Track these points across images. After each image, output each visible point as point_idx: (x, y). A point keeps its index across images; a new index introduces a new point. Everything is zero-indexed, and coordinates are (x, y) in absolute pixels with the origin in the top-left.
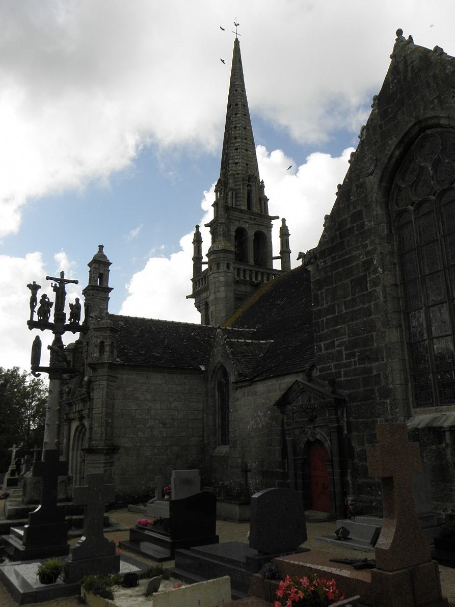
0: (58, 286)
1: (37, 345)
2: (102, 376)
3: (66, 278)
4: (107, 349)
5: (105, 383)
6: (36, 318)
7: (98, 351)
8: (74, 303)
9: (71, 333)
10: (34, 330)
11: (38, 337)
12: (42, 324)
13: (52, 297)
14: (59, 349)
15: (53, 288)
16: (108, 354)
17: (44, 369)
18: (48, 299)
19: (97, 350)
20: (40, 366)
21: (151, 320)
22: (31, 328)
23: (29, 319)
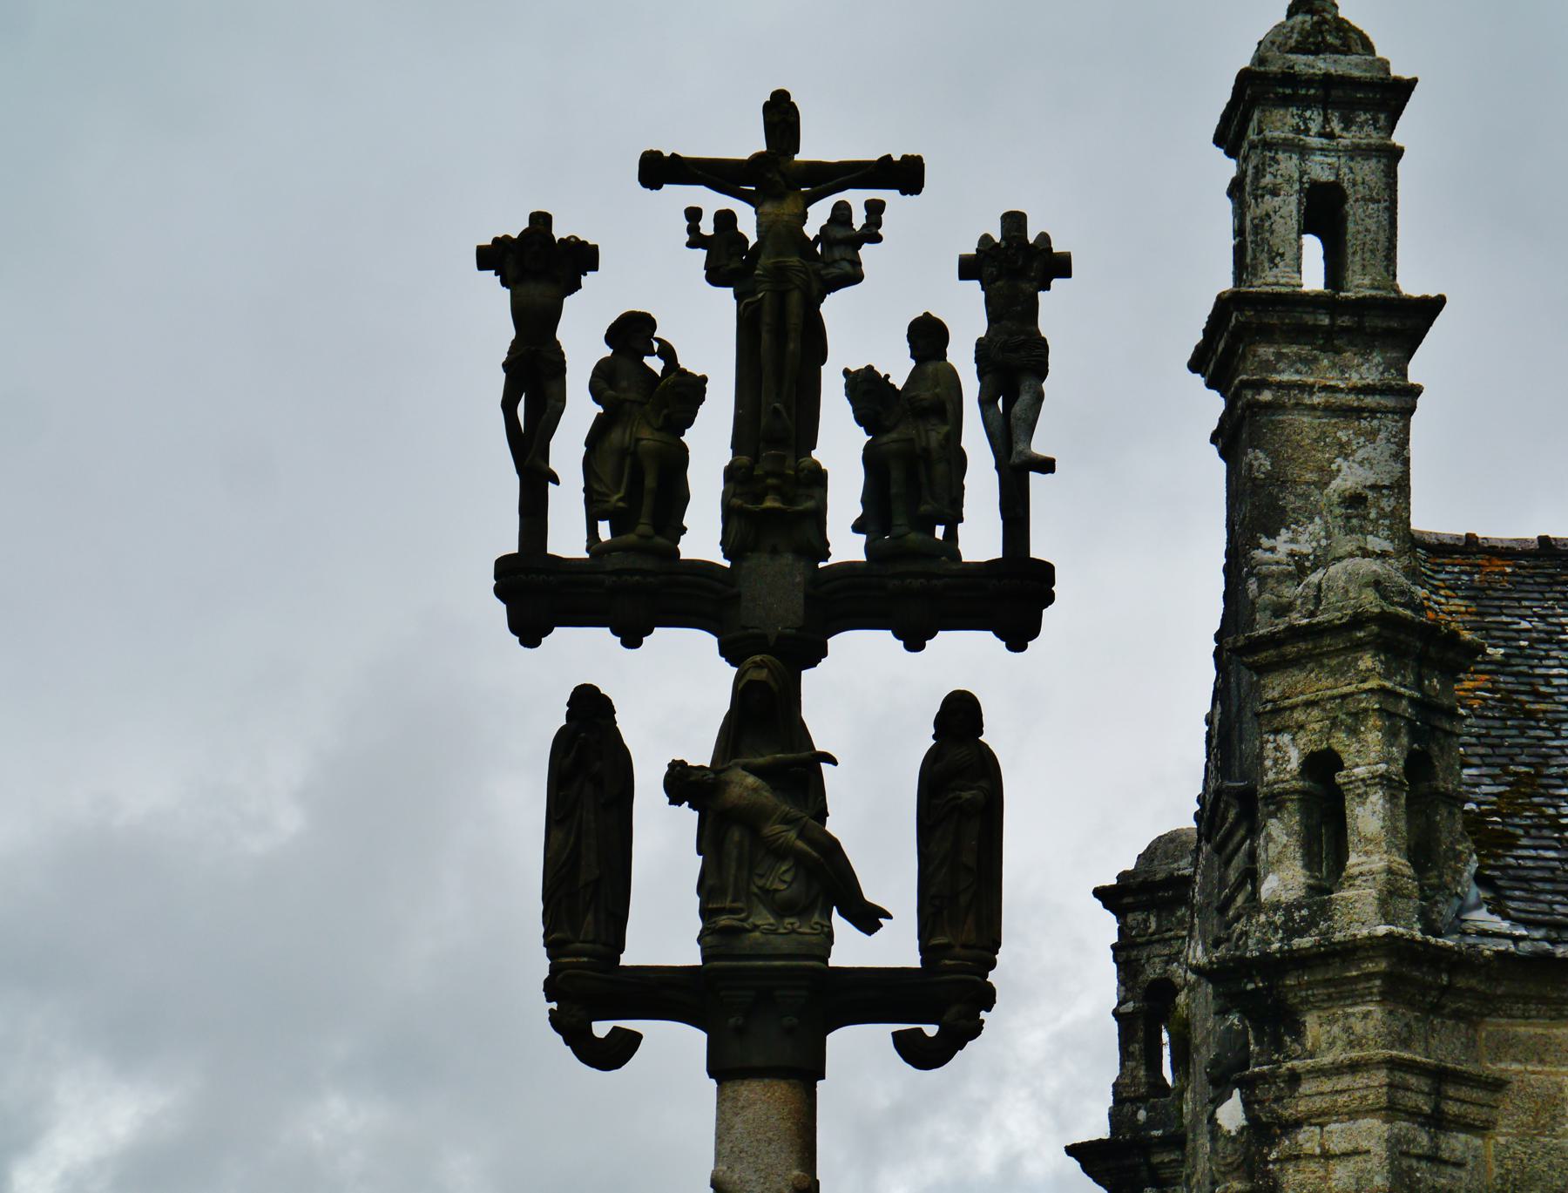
0: (747, 222)
1: (588, 752)
2: (1337, 1070)
3: (811, 149)
4: (1369, 816)
5: (1372, 1132)
6: (568, 535)
7: (1295, 851)
8: (898, 367)
9: (883, 642)
10: (562, 639)
11: (960, 716)
12: (630, 588)
13: (706, 334)
14: (767, 796)
15: (701, 255)
16: (1378, 862)
17: (664, 993)
18: (667, 353)
19: (1521, 944)
20: (626, 960)
21: (1325, 258)
22: (529, 629)
23: (513, 547)
